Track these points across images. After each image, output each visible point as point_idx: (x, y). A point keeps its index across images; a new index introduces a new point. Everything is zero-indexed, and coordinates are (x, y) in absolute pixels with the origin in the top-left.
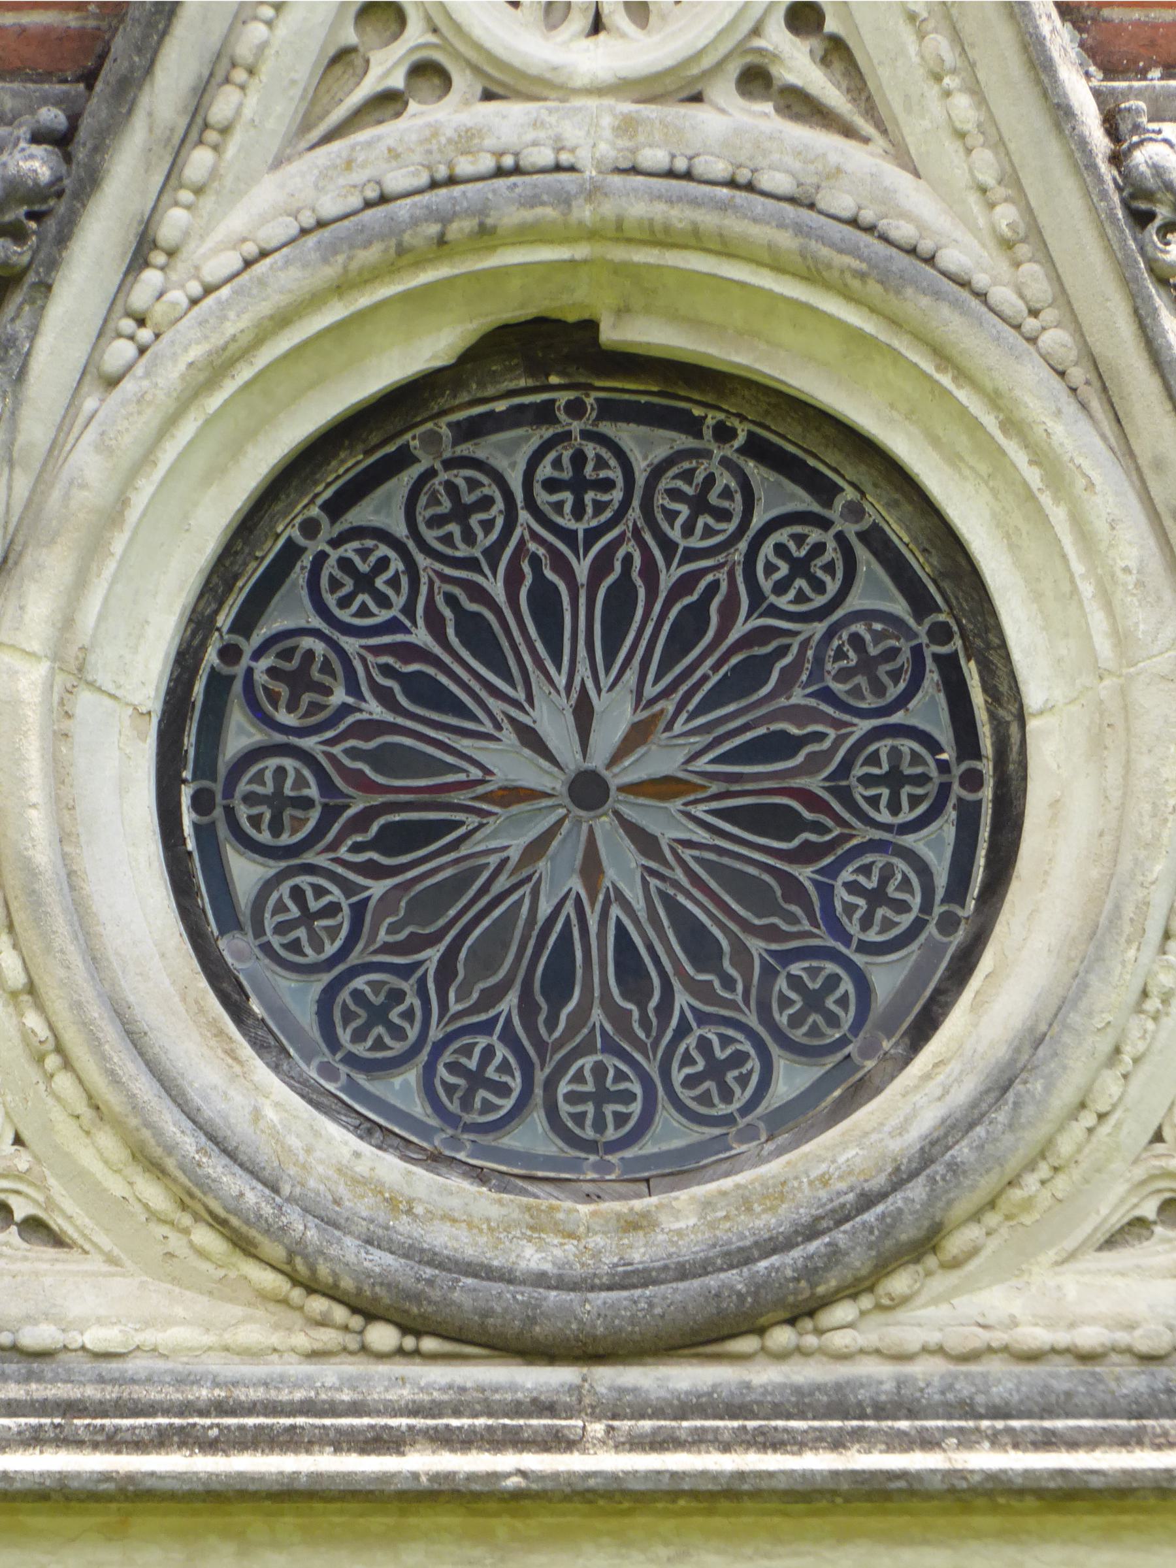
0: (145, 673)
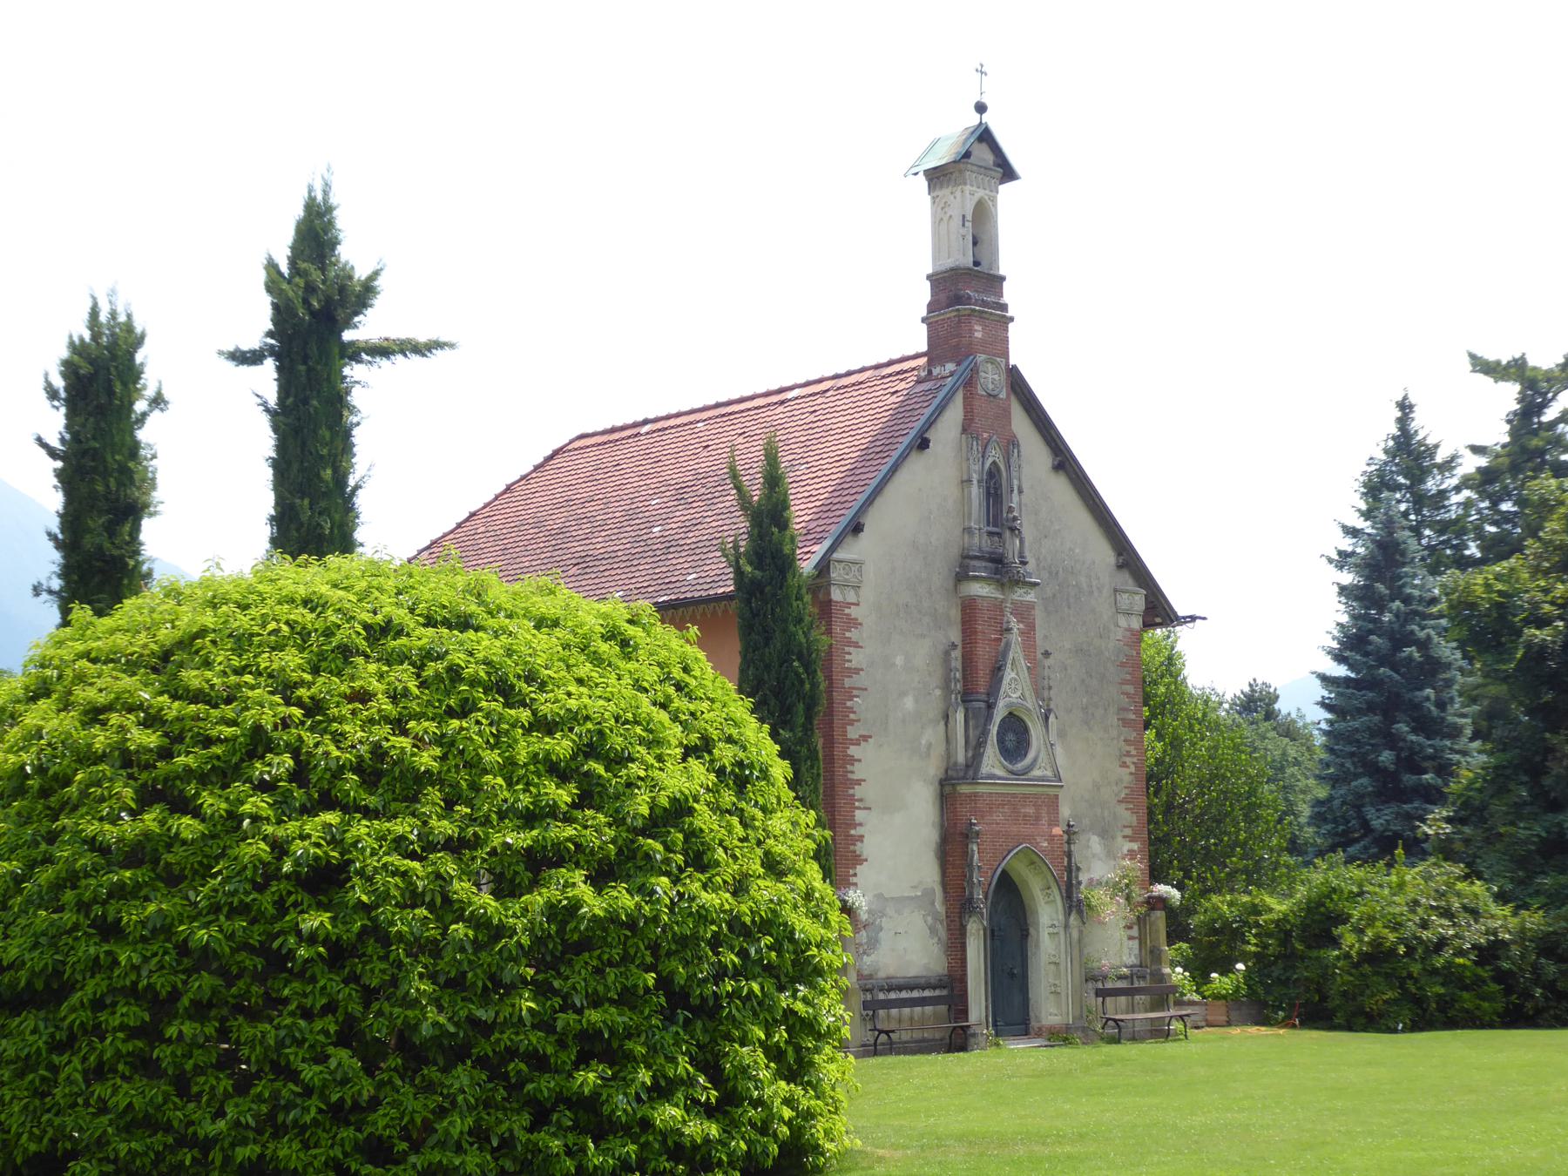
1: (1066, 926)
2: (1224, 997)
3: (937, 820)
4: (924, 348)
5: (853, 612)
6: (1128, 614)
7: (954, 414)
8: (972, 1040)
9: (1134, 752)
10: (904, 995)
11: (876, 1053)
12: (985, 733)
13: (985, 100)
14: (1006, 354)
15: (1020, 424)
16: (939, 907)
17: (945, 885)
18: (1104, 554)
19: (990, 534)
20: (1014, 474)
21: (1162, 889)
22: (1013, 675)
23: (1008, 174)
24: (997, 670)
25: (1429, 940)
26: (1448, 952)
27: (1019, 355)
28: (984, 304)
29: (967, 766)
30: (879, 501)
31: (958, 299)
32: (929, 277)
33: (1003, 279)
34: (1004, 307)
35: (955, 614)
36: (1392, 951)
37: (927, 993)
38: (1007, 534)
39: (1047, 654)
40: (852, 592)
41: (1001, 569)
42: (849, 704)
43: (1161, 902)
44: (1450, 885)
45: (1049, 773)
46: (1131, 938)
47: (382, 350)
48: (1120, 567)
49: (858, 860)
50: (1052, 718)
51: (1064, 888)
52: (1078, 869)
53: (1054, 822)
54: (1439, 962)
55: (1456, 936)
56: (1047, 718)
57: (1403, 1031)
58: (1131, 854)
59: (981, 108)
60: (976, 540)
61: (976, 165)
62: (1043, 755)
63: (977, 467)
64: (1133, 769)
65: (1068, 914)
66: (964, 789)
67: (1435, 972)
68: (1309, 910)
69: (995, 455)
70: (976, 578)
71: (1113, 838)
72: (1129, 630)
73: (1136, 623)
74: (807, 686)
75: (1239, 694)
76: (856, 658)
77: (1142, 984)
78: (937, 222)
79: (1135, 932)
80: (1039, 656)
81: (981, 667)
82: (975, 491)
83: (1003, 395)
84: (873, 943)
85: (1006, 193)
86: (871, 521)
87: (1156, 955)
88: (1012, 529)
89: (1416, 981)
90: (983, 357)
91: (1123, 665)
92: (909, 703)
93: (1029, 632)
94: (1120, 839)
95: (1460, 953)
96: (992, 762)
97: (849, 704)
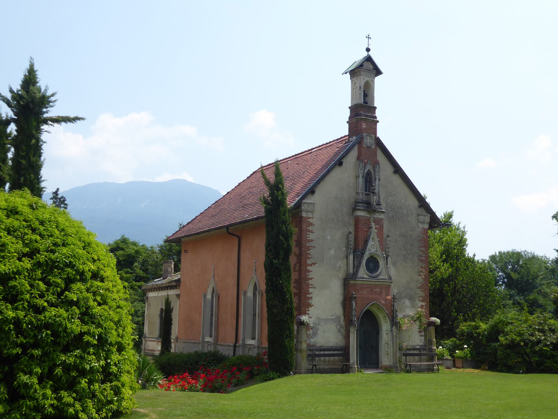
1: (392, 331)
2: (462, 358)
3: (342, 292)
4: (347, 134)
5: (311, 220)
6: (423, 223)
7: (354, 153)
8: (351, 369)
9: (424, 271)
10: (326, 352)
11: (312, 373)
12: (360, 263)
13: (370, 47)
14: (375, 133)
15: (381, 157)
16: (342, 322)
17: (344, 315)
18: (414, 202)
19: (367, 194)
20: (376, 174)
21: (433, 319)
22: (373, 243)
23: (378, 72)
24: (366, 242)
25: (533, 340)
26: (540, 346)
27: (378, 135)
28: (367, 116)
29: (354, 274)
30: (322, 183)
31: (357, 115)
32: (349, 108)
33: (376, 108)
34: (376, 117)
35: (352, 222)
36: (519, 344)
37: (335, 352)
38: (372, 194)
39: (388, 236)
40: (311, 214)
41: (369, 206)
42: (308, 252)
43: (433, 323)
44: (545, 321)
45: (386, 277)
46: (421, 336)
47: (57, 120)
48: (420, 207)
49: (310, 305)
50: (389, 258)
51: (391, 318)
52: (397, 311)
53: (388, 294)
54: (537, 348)
55: (545, 339)
56: (387, 259)
57: (522, 373)
58: (422, 307)
59: (368, 50)
60: (361, 196)
61: (366, 70)
62: (384, 271)
63: (362, 172)
64: (423, 277)
65: (392, 327)
66: (352, 282)
67: (536, 352)
68: (493, 329)
69: (369, 167)
70: (359, 210)
71: (415, 301)
72: (423, 228)
73: (426, 226)
74: (285, 245)
75: (554, 258)
76: (311, 236)
77: (425, 352)
78: (353, 89)
79: (423, 334)
80: (385, 236)
81: (360, 240)
82: (361, 180)
83: (373, 147)
84: (315, 334)
85: (378, 79)
86: (318, 191)
87: (430, 342)
88: (373, 193)
89: (528, 355)
90: (366, 134)
91: (420, 240)
92: (332, 252)
93: (380, 228)
95: (546, 345)
96: (363, 272)
97: (308, 252)
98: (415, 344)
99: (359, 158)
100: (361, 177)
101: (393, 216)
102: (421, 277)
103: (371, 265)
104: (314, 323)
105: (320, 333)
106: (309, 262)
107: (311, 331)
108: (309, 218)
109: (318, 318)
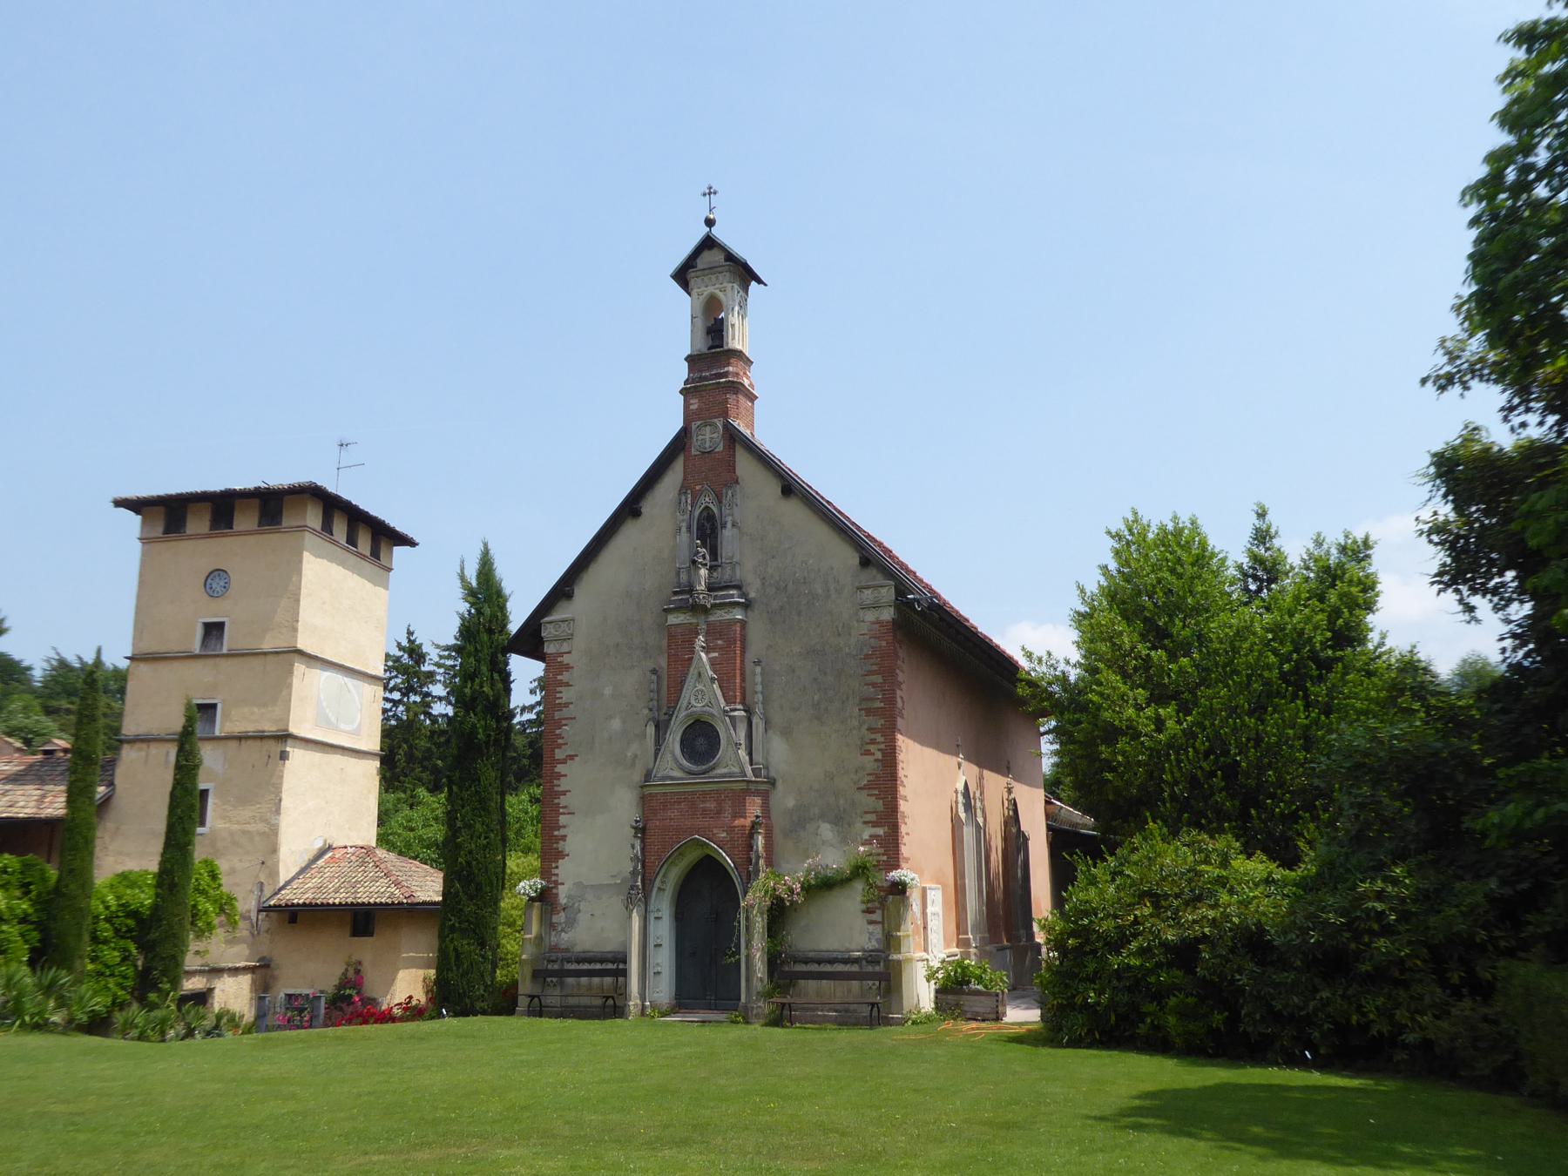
0: (678, 738)
5: (566, 659)
6: (875, 606)
18: (630, 532)
22: (700, 687)
45: (736, 770)
46: (871, 922)
54: (1115, 962)
59: (710, 223)
63: (686, 517)
64: (879, 755)
69: (707, 500)
83: (720, 448)
84: (571, 923)
91: (867, 657)
92: (616, 724)
94: (859, 825)
96: (673, 764)
98: (853, 947)
99: (683, 490)
100: (684, 529)
101: (782, 608)
102: (871, 758)
103: (701, 743)
104: (569, 897)
105: (583, 918)
106: (559, 754)
107: (562, 914)
108: (561, 654)
109: (578, 885)
